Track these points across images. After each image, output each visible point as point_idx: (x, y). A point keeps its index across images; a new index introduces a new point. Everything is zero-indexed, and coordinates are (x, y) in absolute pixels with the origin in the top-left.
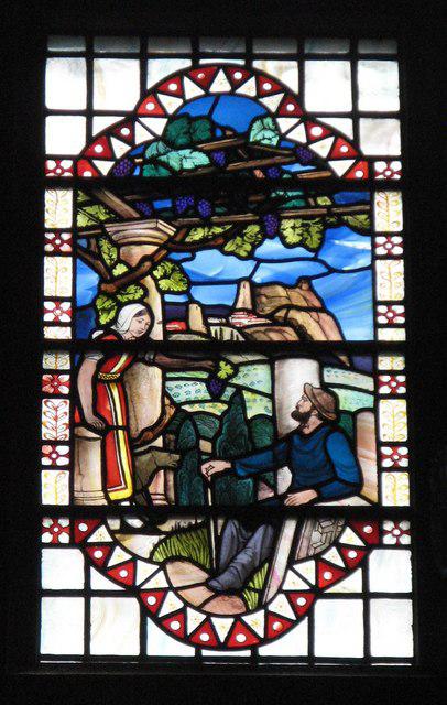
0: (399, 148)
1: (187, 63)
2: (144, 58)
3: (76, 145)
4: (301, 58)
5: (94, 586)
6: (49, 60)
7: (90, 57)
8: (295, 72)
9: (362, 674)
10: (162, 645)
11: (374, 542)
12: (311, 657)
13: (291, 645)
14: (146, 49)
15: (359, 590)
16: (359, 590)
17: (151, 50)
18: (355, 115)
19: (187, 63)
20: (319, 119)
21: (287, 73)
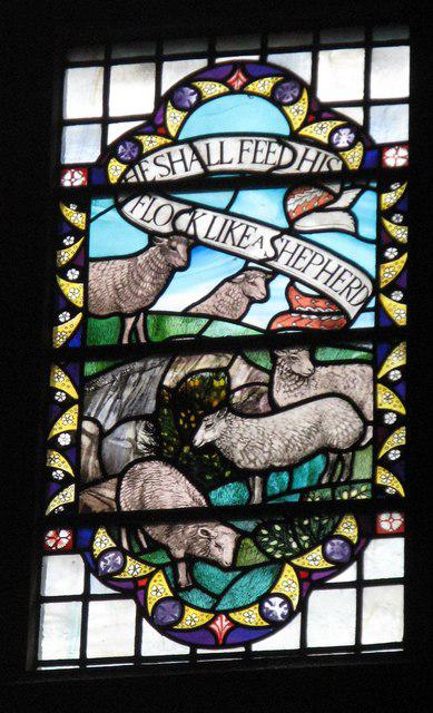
0: (407, 131)
1: (201, 63)
2: (158, 61)
3: (91, 154)
4: (315, 50)
5: (93, 591)
6: (70, 70)
7: (107, 66)
8: (309, 63)
9: (356, 661)
10: (157, 645)
11: (370, 532)
12: (358, 646)
13: (286, 640)
14: (319, 39)
15: (80, 604)
16: (80, 604)
17: (115, 56)
18: (105, 121)
19: (201, 63)
20: (339, 110)
21: (299, 64)
